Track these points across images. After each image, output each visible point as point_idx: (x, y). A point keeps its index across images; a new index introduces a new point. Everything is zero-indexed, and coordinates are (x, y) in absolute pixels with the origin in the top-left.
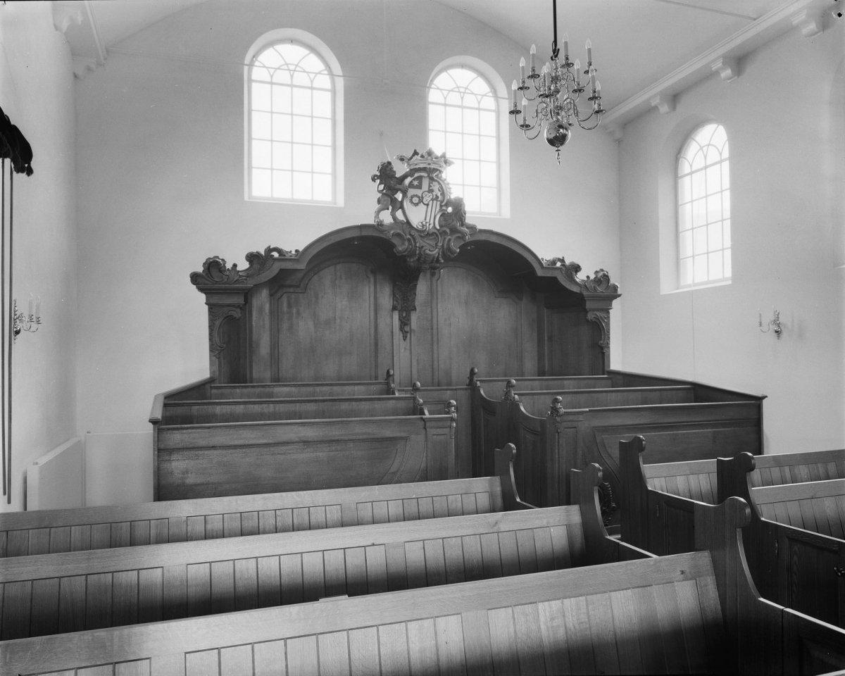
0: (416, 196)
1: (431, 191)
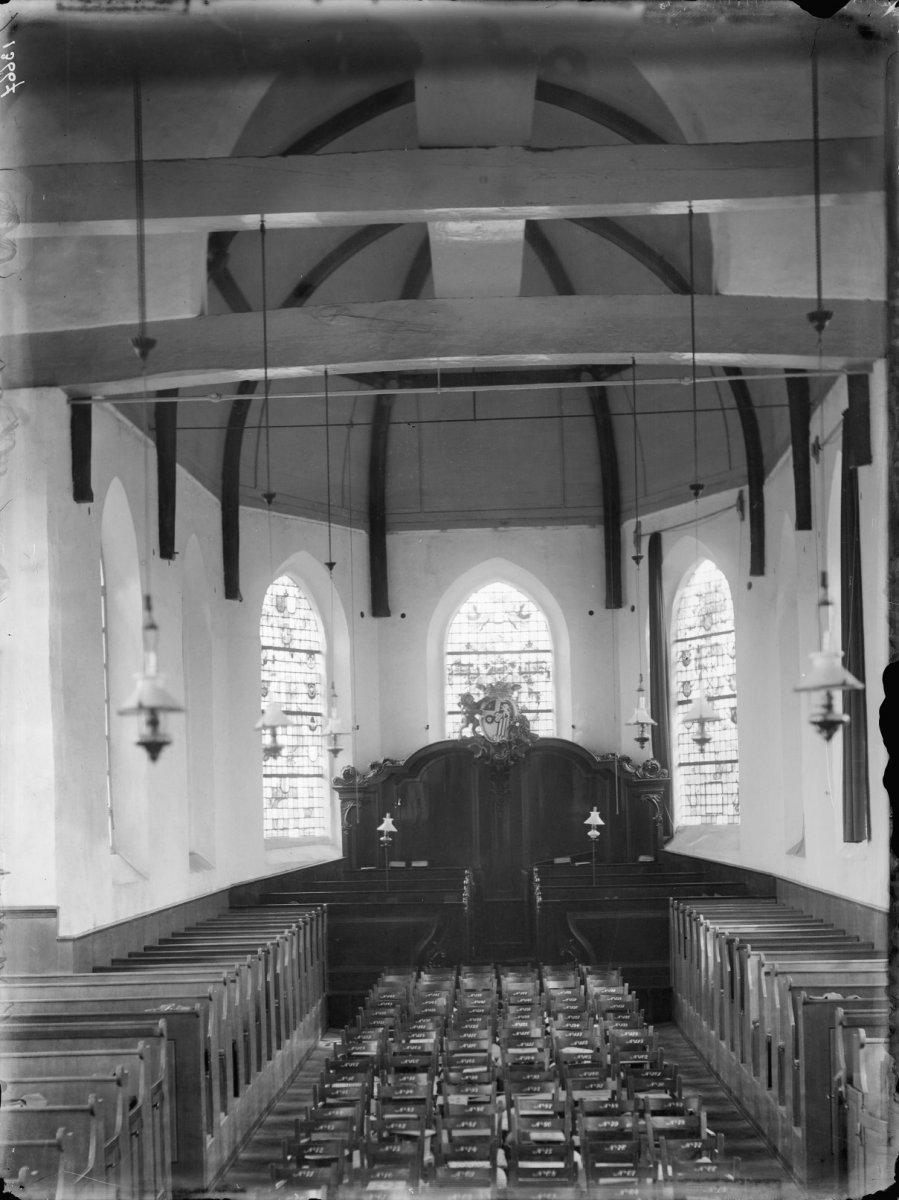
0: (490, 716)
1: (501, 712)
